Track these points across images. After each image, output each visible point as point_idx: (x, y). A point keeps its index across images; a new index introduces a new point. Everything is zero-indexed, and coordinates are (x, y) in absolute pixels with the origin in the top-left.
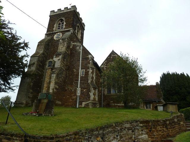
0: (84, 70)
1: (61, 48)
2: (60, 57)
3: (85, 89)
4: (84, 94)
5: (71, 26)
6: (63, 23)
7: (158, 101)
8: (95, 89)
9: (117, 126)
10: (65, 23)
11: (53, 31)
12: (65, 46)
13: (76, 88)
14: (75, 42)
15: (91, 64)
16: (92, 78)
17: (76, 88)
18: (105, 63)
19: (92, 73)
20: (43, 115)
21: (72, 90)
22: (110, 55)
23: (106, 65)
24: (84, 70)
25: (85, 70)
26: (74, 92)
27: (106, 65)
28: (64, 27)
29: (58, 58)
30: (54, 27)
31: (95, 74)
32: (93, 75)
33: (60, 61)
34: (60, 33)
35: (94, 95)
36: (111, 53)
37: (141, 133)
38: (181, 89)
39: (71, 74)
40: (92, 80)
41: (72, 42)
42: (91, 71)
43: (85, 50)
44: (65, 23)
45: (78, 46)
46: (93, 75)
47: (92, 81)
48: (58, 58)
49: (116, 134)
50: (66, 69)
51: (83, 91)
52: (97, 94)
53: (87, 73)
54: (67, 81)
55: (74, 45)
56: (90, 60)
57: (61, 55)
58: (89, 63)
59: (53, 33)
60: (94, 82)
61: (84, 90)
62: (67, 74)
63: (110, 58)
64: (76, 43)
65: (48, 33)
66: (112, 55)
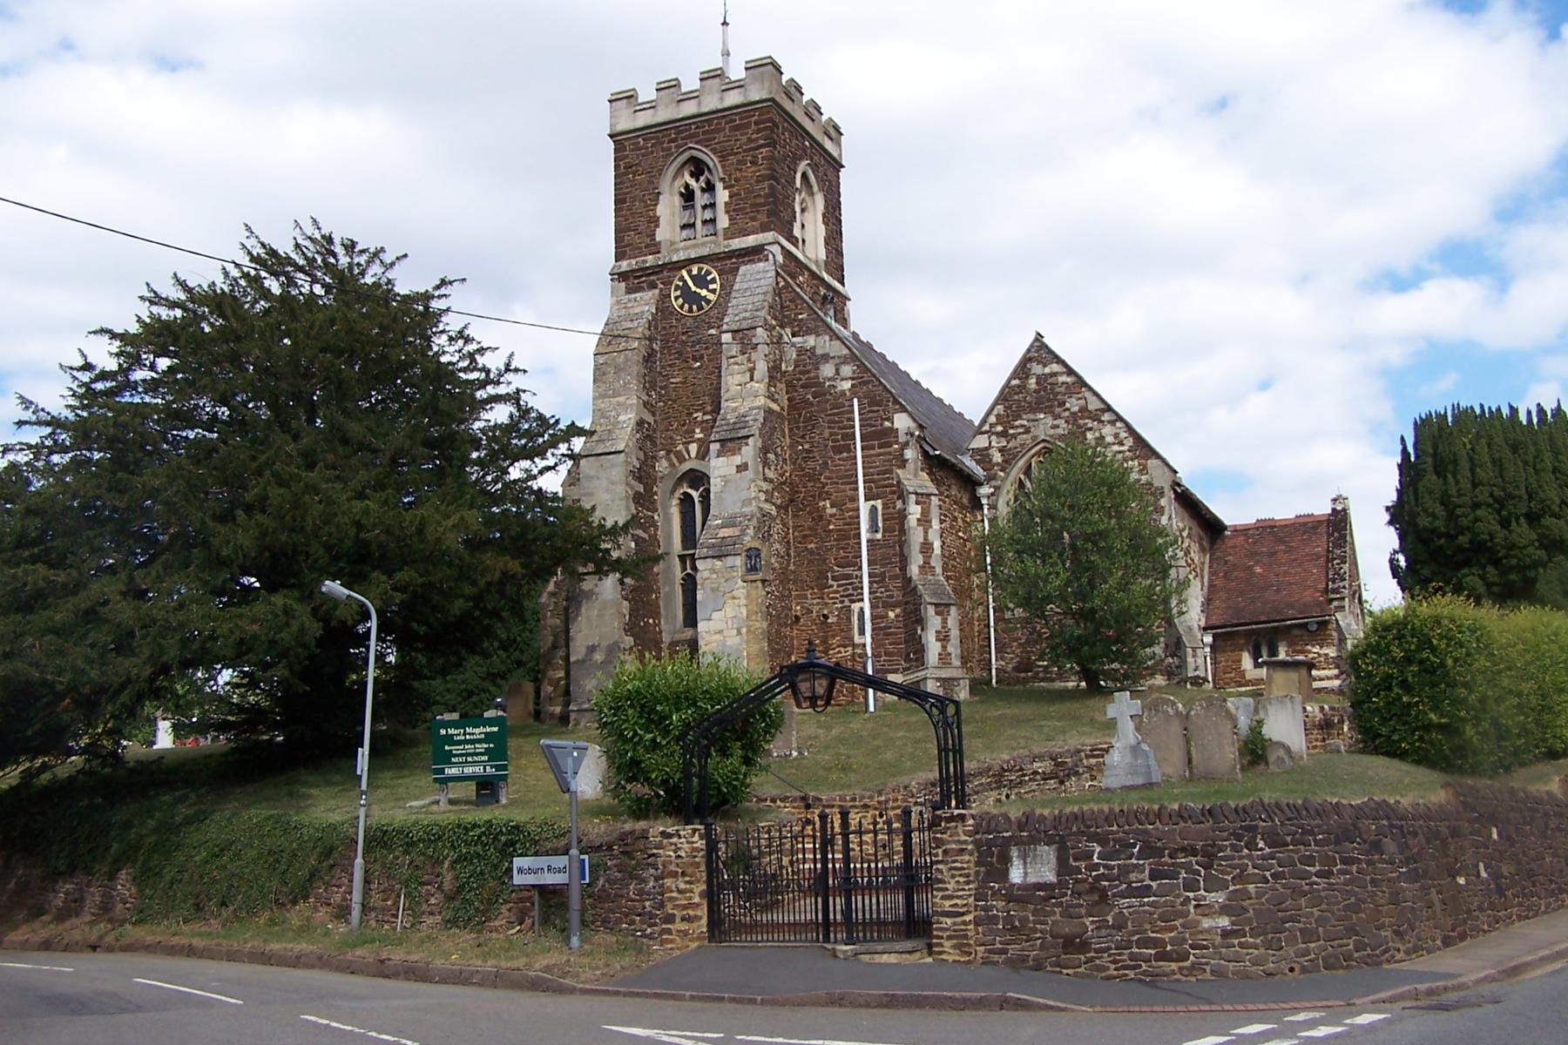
0: (879, 504)
1: (735, 389)
2: (749, 452)
3: (893, 606)
4: (890, 634)
5: (763, 218)
6: (709, 188)
7: (1318, 623)
8: (942, 609)
9: (1006, 771)
10: (722, 195)
11: (655, 248)
12: (757, 375)
13: (847, 603)
14: (809, 332)
15: (910, 466)
16: (926, 548)
17: (847, 603)
18: (992, 419)
19: (925, 521)
20: (32, 701)
21: (826, 617)
22: (1022, 370)
23: (998, 434)
24: (879, 504)
25: (885, 506)
26: (838, 624)
27: (1003, 434)
28: (723, 222)
29: (737, 460)
30: (655, 221)
31: (936, 525)
32: (926, 532)
33: (749, 474)
34: (706, 267)
35: (943, 638)
36: (1029, 350)
37: (1087, 785)
38: (1506, 524)
39: (810, 528)
40: (926, 563)
41: (788, 331)
42: (915, 511)
43: (863, 358)
44: (722, 195)
45: (826, 358)
46: (926, 532)
47: (926, 567)
48: (737, 460)
49: (1005, 791)
50: (778, 507)
51: (887, 616)
52: (955, 633)
53: (896, 522)
54: (792, 567)
55: (801, 351)
56: (906, 444)
57: (750, 441)
58: (903, 463)
59: (658, 269)
60: (939, 570)
61: (891, 615)
62: (788, 533)
63: (1022, 388)
64: (811, 341)
65: (625, 265)
66: (1037, 369)
